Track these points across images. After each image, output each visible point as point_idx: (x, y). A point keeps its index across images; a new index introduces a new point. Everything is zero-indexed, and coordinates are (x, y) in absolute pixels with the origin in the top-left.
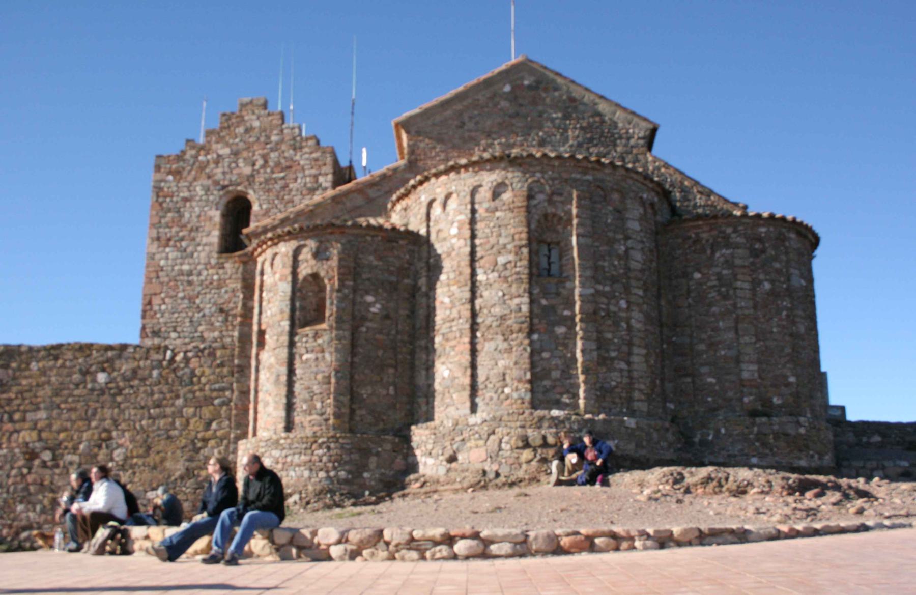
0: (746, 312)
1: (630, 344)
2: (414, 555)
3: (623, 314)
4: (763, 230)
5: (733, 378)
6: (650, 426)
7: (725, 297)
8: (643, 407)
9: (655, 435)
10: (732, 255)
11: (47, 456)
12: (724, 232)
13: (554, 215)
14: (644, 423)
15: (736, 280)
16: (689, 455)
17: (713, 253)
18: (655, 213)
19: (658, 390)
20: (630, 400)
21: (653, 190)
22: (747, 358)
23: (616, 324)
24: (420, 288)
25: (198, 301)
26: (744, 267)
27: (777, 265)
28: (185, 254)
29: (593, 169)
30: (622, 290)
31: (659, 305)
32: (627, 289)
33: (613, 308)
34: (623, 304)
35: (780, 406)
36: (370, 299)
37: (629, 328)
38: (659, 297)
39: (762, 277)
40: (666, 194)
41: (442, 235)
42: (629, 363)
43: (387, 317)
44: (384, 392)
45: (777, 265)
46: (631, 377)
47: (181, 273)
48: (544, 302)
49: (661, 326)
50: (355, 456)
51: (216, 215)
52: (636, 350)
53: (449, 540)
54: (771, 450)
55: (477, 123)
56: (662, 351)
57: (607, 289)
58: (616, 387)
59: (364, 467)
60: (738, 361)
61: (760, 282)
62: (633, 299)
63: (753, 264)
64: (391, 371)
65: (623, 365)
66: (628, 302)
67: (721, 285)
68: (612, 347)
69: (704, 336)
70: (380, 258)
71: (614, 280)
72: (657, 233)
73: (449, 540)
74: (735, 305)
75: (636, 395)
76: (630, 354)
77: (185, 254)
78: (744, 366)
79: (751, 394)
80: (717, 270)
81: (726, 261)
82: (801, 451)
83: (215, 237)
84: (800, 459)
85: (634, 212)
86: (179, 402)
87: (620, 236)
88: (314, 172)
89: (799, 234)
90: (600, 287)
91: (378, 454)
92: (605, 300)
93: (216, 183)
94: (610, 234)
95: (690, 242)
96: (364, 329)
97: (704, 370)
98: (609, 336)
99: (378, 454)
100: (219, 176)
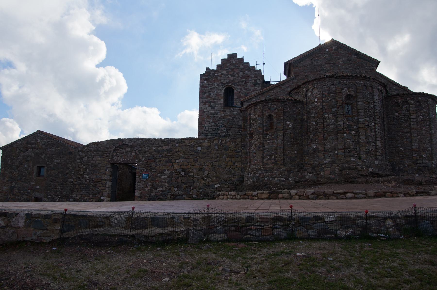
0: (414, 126)
1: (376, 137)
2: (335, 198)
3: (373, 127)
4: (420, 98)
5: (409, 148)
6: (382, 164)
7: (406, 121)
8: (380, 157)
9: (384, 167)
10: (409, 107)
11: (183, 173)
12: (406, 99)
13: (350, 95)
14: (381, 163)
15: (410, 115)
16: (394, 174)
17: (402, 106)
18: (382, 93)
19: (384, 152)
20: (376, 155)
21: (382, 86)
22: (414, 141)
23: (371, 131)
24: (304, 119)
25: (217, 123)
26: (413, 111)
27: (425, 110)
28: (213, 108)
29: (363, 79)
30: (373, 119)
31: (384, 124)
32: (374, 119)
33: (370, 126)
34: (373, 124)
35: (425, 158)
36: (288, 123)
37: (375, 131)
38: (384, 121)
39: (419, 114)
40: (385, 86)
41: (311, 102)
42: (375, 143)
43: (294, 128)
44: (294, 153)
45: (425, 110)
46: (376, 148)
47: (211, 114)
48: (348, 123)
49: (385, 131)
50: (286, 173)
51: (222, 94)
52: (377, 139)
53: (345, 193)
54: (423, 172)
55: (317, 62)
56: (385, 140)
57: (368, 119)
58: (371, 151)
59: (289, 177)
60: (411, 142)
61: (419, 116)
62: (376, 122)
63: (416, 110)
64: (296, 146)
65: (373, 144)
66: (375, 123)
67: (405, 117)
68: (370, 138)
69: (399, 134)
70: (290, 109)
71: (370, 116)
72: (383, 100)
73: (345, 193)
74: (410, 124)
75: (378, 154)
76: (376, 140)
77: (213, 108)
78: (413, 144)
79: (415, 154)
80: (403, 112)
81: (407, 109)
82: (433, 172)
83: (222, 101)
84: (433, 175)
85: (376, 93)
86: (83, 165)
87: (372, 102)
88: (256, 78)
89: (432, 99)
90: (366, 119)
91: (293, 172)
92: (367, 123)
93: (221, 83)
94: (369, 101)
95: (394, 103)
96: (287, 132)
97: (399, 145)
98: (369, 134)
99: (293, 172)
100: (222, 81)
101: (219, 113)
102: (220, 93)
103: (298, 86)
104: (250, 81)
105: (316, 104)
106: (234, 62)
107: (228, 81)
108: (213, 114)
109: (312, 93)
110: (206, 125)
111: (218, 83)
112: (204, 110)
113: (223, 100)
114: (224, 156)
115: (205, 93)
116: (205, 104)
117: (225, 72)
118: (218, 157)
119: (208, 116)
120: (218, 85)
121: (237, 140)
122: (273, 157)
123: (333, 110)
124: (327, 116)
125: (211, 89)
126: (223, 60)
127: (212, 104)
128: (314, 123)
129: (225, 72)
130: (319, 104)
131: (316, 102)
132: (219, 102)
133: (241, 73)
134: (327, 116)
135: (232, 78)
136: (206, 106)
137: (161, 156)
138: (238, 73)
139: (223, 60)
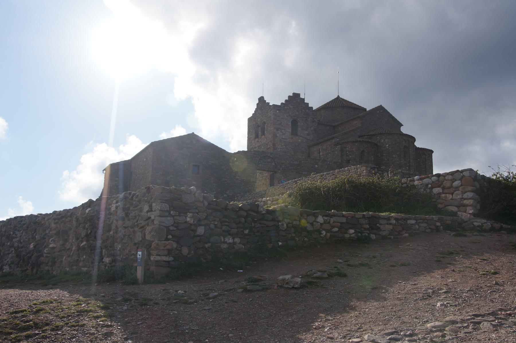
28: (284, 134)
47: (283, 138)
51: (290, 124)
100: (290, 114)
108: (284, 139)
109: (384, 140)
120: (287, 116)
123: (398, 153)
126: (308, 104)
127: (283, 131)
135: (297, 113)
139: (308, 104)
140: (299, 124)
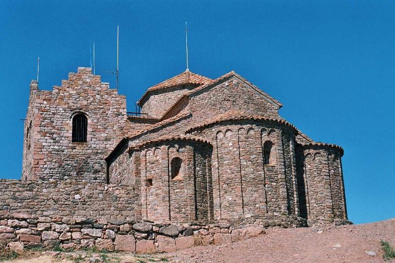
13: (269, 141)
51: (71, 122)
93: (69, 107)
100: (71, 104)
101: (66, 151)
102: (68, 122)
103: (205, 125)
104: (111, 110)
105: (231, 148)
106: (88, 80)
107: (79, 106)
110: (45, 166)
111: (64, 106)
112: (44, 144)
113: (71, 132)
114: (113, 208)
115: (45, 119)
116: (45, 136)
117: (75, 92)
118: (103, 210)
119: (50, 152)
121: (128, 188)
122: (183, 210)
124: (245, 163)
125: (54, 114)
128: (228, 171)
129: (75, 92)
130: (235, 149)
131: (231, 146)
132: (65, 135)
133: (98, 96)
134: (245, 163)
136: (46, 138)
137: (20, 205)
138: (93, 96)
140: (89, 121)
